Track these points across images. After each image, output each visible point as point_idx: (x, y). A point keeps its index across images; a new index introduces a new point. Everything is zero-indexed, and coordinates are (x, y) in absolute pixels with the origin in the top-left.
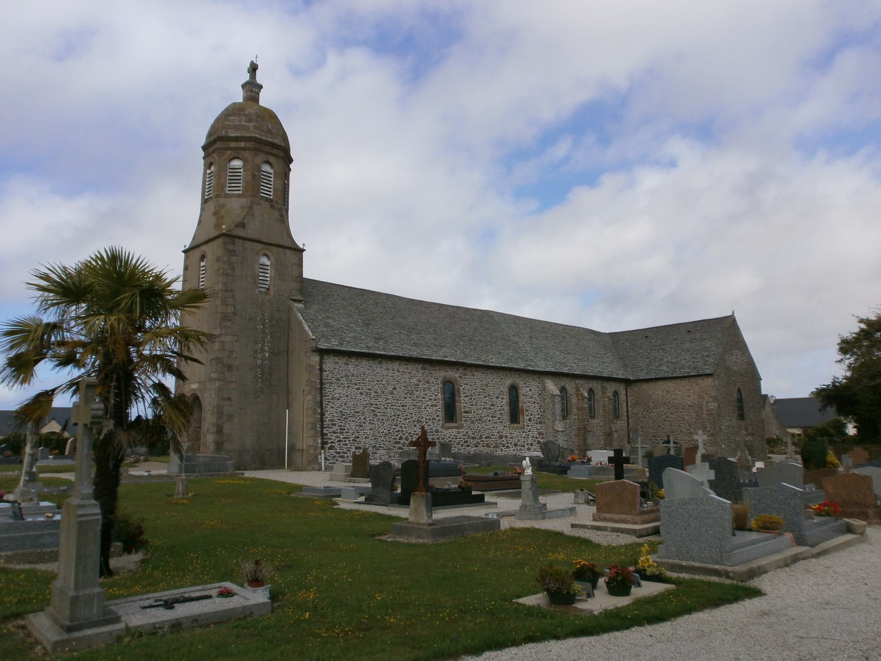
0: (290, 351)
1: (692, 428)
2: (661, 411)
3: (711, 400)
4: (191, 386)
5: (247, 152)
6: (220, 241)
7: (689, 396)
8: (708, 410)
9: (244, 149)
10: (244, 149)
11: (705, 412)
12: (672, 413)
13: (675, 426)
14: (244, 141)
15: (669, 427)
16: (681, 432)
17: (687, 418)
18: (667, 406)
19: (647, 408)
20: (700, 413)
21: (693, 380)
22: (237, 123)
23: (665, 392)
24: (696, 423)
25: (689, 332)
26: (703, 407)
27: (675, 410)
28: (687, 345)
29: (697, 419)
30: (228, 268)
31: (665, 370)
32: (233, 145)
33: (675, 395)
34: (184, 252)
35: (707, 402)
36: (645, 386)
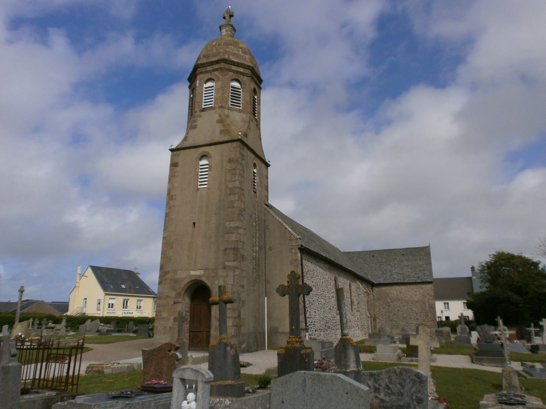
0: (268, 246)
1: (418, 316)
2: (396, 305)
3: (431, 298)
4: (190, 272)
5: (245, 77)
6: (235, 144)
7: (416, 295)
8: (429, 304)
9: (243, 74)
10: (243, 74)
11: (427, 306)
12: (404, 306)
13: (406, 314)
14: (243, 68)
15: (402, 315)
16: (411, 318)
17: (414, 309)
18: (401, 301)
19: (386, 302)
20: (424, 306)
21: (419, 286)
22: (236, 52)
23: (399, 292)
24: (421, 312)
25: (403, 254)
26: (426, 303)
27: (406, 304)
28: (406, 263)
29: (422, 310)
30: (242, 169)
31: (397, 278)
32: (234, 68)
33: (406, 294)
34: (172, 150)
35: (429, 300)
36: (384, 288)
